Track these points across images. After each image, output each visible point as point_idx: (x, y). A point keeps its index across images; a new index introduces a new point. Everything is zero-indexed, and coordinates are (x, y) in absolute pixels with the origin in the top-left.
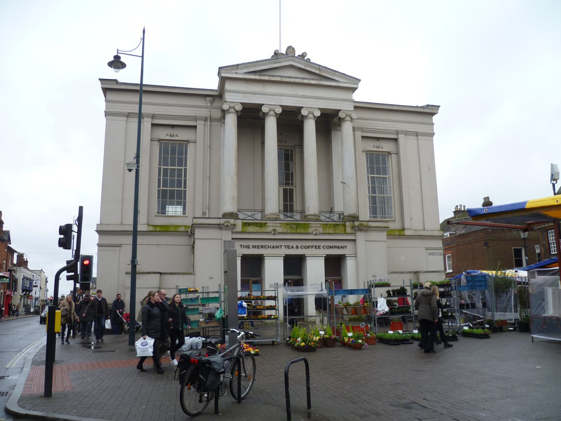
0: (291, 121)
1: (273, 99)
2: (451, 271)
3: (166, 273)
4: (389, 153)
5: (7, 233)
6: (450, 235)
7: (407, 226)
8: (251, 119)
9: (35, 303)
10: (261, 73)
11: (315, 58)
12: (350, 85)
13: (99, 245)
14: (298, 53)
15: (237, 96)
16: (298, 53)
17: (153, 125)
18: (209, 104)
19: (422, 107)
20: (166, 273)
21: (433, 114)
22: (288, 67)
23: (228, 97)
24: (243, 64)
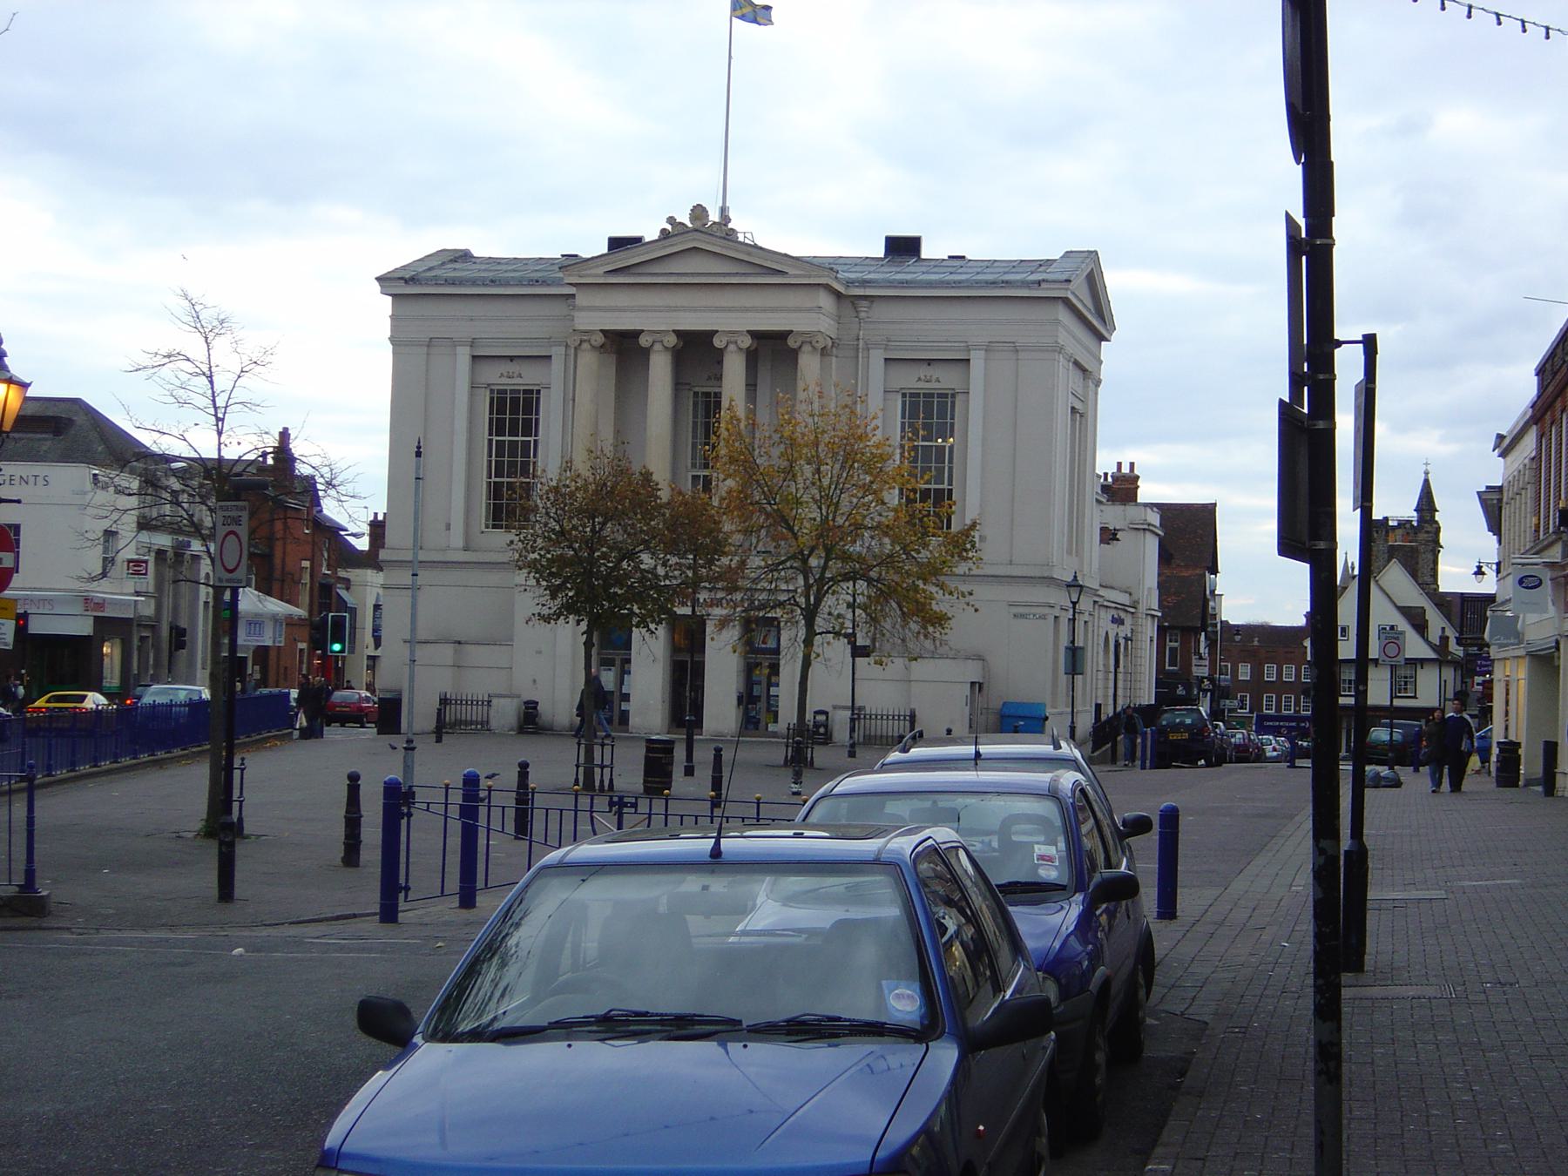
0: (695, 351)
1: (658, 316)
8: (624, 349)
17: (474, 357)
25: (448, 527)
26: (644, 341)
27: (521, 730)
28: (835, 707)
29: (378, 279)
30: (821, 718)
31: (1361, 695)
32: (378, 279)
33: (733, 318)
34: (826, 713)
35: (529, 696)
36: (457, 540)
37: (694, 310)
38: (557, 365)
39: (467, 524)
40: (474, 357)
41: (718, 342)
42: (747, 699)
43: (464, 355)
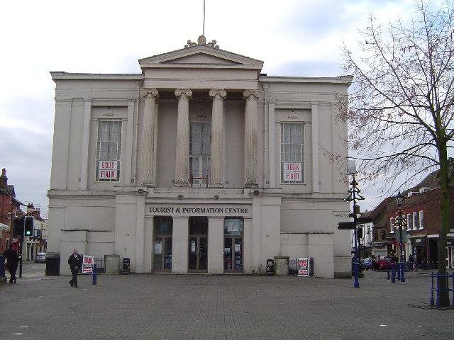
0: (201, 100)
1: (185, 83)
2: (422, 228)
3: (92, 231)
4: (304, 123)
5: (12, 187)
6: (425, 190)
7: (316, 189)
8: (166, 99)
9: (417, 238)
10: (171, 62)
11: (224, 45)
12: (255, 67)
13: (50, 207)
14: (209, 40)
15: (157, 82)
16: (209, 40)
17: (92, 107)
18: (138, 88)
19: (336, 79)
20: (92, 231)
21: (348, 85)
22: (203, 54)
23: (148, 84)
24: (144, 59)
25: (80, 180)
26: (211, 94)
27: (121, 273)
28: (276, 258)
29: (60, 78)
30: (270, 263)
31: (388, 273)
32: (60, 78)
33: (218, 84)
34: (271, 260)
35: (124, 256)
36: (83, 185)
37: (155, 79)
38: (131, 109)
39: (88, 178)
40: (92, 107)
41: (177, 93)
42: (192, 257)
43: (88, 106)
